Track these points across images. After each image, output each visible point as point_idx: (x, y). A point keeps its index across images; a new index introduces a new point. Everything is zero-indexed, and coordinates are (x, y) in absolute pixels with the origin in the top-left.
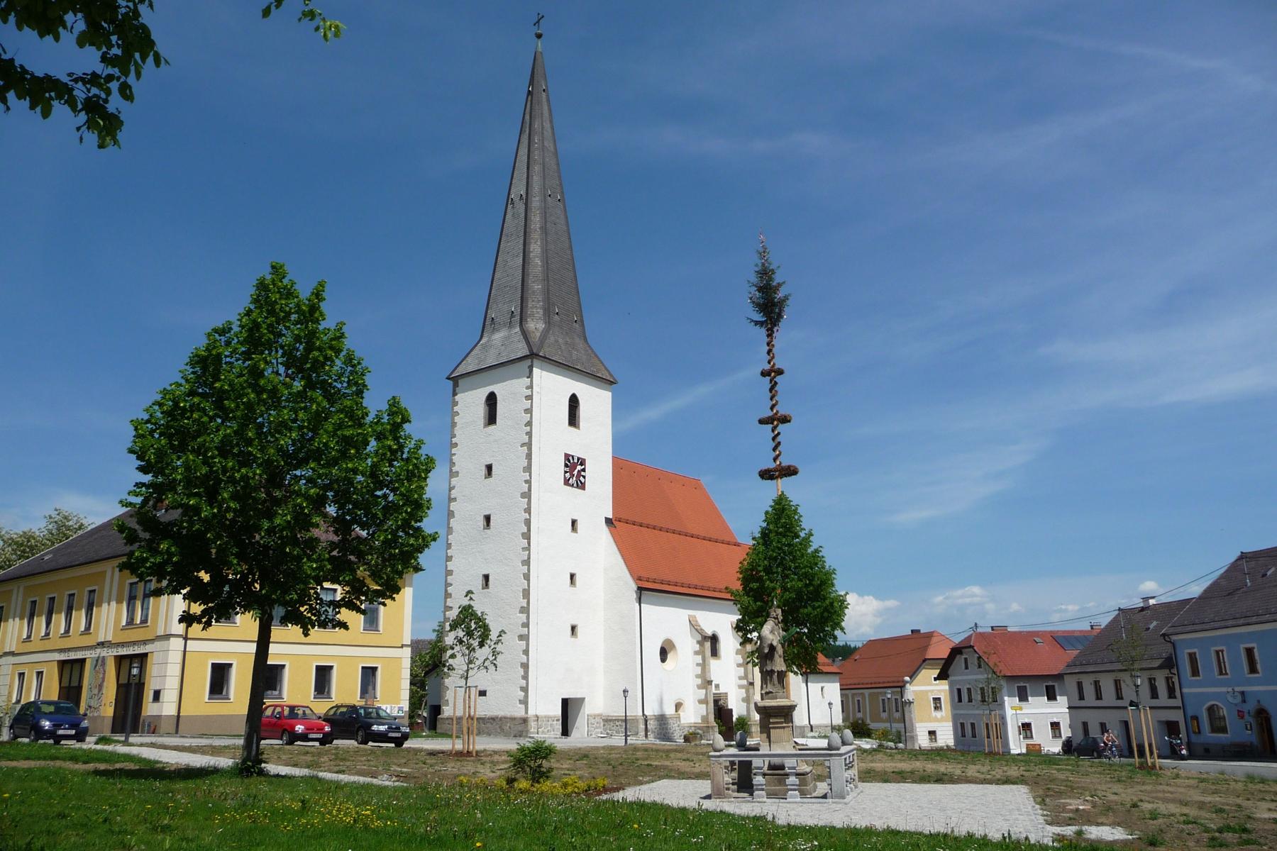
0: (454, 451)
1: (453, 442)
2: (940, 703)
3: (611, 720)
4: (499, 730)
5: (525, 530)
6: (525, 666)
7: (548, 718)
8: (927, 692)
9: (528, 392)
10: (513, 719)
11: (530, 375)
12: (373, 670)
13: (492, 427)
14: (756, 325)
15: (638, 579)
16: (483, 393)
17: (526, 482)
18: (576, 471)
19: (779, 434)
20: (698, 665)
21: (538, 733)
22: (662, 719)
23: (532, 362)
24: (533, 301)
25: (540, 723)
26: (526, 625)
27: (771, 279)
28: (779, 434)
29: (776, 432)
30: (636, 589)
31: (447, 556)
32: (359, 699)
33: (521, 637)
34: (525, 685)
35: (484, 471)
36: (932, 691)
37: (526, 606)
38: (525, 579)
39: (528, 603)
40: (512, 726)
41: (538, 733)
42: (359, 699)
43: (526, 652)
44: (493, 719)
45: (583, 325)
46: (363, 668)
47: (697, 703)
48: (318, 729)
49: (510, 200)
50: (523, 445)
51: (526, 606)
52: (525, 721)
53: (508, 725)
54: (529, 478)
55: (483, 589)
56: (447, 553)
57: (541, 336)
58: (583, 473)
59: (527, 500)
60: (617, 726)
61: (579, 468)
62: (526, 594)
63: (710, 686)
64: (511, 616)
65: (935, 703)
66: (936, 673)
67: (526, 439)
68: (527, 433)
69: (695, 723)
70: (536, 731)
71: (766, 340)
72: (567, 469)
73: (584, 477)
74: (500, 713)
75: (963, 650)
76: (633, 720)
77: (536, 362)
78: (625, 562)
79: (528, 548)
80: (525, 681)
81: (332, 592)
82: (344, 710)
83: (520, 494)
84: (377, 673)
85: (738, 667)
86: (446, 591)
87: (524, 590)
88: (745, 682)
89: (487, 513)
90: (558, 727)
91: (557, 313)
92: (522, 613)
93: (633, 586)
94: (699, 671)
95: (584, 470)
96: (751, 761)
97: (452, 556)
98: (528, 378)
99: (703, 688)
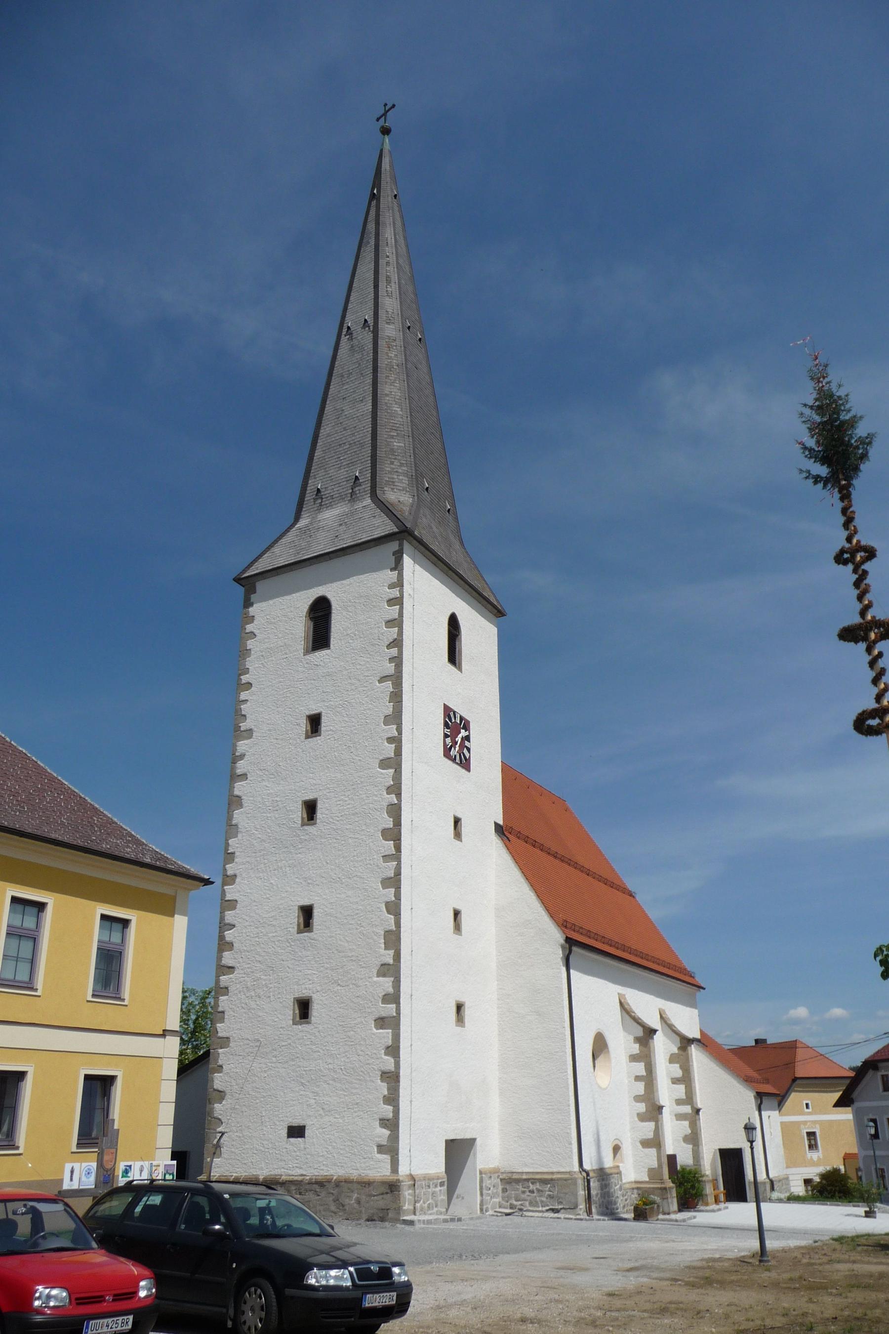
0: (243, 696)
1: (243, 681)
2: (815, 1140)
3: (518, 1181)
4: (333, 1208)
5: (390, 824)
6: (392, 1078)
7: (428, 1178)
8: (798, 1124)
9: (395, 593)
10: (366, 1184)
11: (398, 565)
12: (107, 1082)
13: (322, 654)
14: (816, 483)
15: (563, 925)
16: (304, 599)
17: (390, 740)
18: (460, 736)
19: (880, 655)
20: (638, 1078)
21: (415, 1214)
22: (603, 1175)
23: (401, 545)
24: (392, 463)
25: (417, 1191)
26: (394, 998)
27: (837, 411)
28: (880, 655)
29: (876, 652)
30: (562, 941)
31: (226, 876)
32: (74, 1149)
33: (381, 1022)
34: (390, 1115)
35: (304, 725)
36: (805, 1123)
37: (391, 962)
38: (389, 912)
39: (397, 957)
40: (364, 1198)
41: (415, 1214)
42: (74, 1149)
43: (394, 1050)
44: (321, 1184)
45: (455, 514)
46: (88, 1078)
47: (640, 1147)
48: (118, 1298)
49: (345, 330)
50: (382, 679)
51: (391, 962)
52: (393, 1187)
53: (355, 1196)
54: (396, 734)
55: (300, 932)
56: (225, 870)
57: (410, 510)
58: (467, 743)
59: (392, 771)
60: (532, 1192)
61: (463, 733)
62: (393, 939)
63: (661, 1116)
64: (360, 983)
65: (809, 1140)
66: (837, 1096)
67: (390, 668)
68: (391, 660)
69: (636, 1182)
70: (411, 1208)
71: (840, 505)
72: (448, 731)
73: (469, 750)
74: (336, 1172)
75: (881, 1065)
76: (566, 1180)
77: (406, 546)
78: (538, 896)
79: (397, 855)
80: (390, 1108)
81: (35, 910)
82: (156, 1200)
83: (377, 761)
84: (113, 1088)
85: (673, 1083)
86: (221, 938)
87: (388, 933)
88: (687, 1109)
89: (310, 797)
90: (442, 1197)
91: (427, 489)
92: (384, 975)
93: (557, 936)
94: (640, 1088)
95: (467, 738)
96: (77, 1149)
97: (235, 876)
98: (392, 570)
99: (649, 1120)
